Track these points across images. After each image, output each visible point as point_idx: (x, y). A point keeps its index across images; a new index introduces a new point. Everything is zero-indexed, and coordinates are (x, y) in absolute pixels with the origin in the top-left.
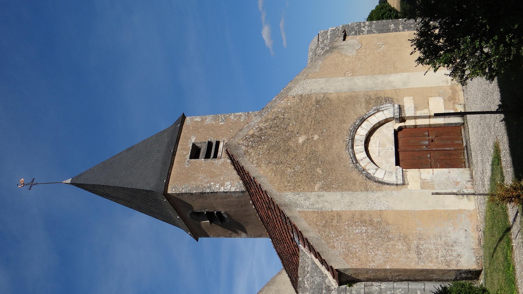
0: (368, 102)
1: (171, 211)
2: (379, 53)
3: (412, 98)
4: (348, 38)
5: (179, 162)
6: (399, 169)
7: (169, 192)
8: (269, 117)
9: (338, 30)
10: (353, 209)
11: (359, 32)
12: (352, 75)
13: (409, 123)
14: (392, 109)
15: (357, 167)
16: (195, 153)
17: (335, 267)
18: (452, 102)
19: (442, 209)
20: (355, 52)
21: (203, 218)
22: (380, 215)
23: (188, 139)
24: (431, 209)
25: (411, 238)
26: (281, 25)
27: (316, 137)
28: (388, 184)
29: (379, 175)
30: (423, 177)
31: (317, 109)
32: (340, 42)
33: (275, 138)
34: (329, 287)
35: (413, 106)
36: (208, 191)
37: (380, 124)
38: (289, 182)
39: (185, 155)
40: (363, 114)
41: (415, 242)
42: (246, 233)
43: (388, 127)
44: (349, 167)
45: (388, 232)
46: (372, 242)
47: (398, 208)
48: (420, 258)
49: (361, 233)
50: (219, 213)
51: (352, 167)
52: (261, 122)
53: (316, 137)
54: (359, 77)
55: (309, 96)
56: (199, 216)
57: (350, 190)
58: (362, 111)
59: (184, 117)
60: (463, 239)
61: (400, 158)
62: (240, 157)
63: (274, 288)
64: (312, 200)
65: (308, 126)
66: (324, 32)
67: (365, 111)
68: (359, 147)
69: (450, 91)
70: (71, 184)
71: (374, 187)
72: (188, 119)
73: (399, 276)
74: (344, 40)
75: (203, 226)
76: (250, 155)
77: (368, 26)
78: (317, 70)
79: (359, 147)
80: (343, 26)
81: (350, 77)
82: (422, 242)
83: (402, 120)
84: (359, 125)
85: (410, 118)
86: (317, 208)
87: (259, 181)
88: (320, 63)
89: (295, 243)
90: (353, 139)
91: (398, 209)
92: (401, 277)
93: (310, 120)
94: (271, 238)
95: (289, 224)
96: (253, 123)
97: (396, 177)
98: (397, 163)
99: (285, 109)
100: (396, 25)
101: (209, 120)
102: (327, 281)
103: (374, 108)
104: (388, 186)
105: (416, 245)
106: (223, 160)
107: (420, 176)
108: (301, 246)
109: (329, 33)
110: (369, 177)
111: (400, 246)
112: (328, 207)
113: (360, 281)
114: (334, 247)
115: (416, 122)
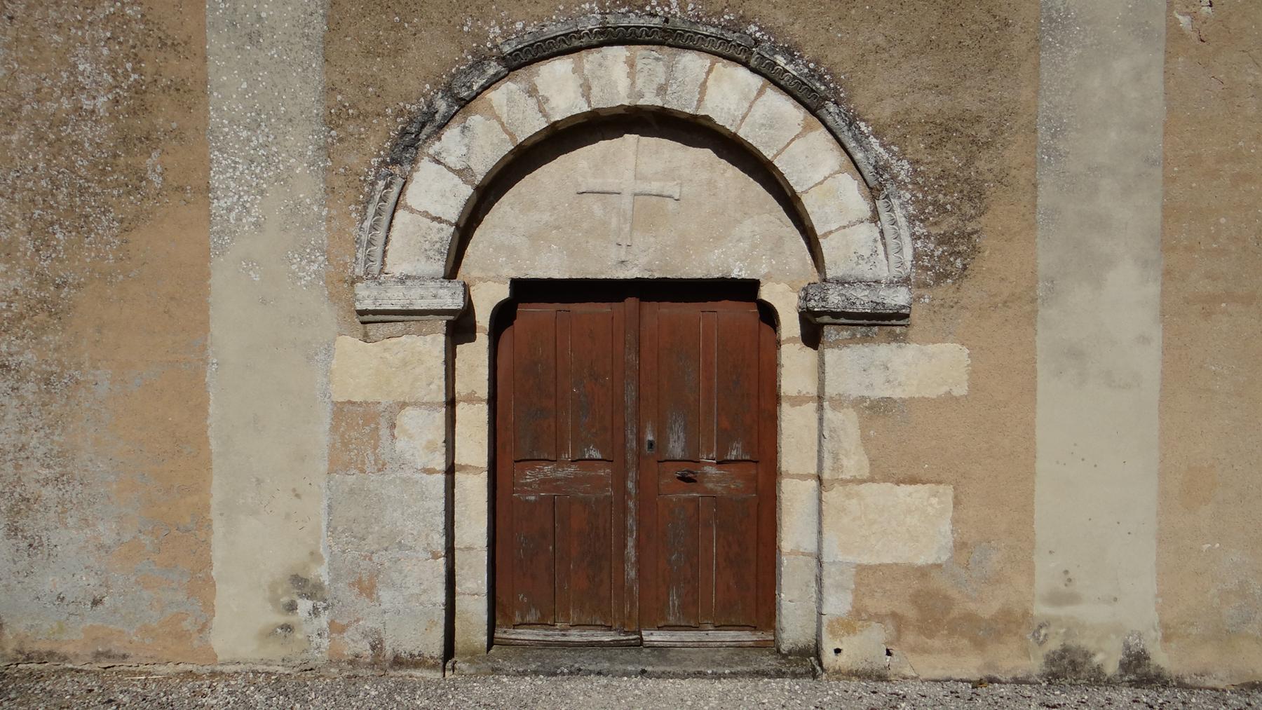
0: (943, 131)
3: (961, 390)
10: (215, 43)
12: (1175, 34)
13: (795, 365)
18: (911, 613)
19: (214, 502)
22: (181, 189)
24: (214, 445)
30: (410, 419)
35: (897, 394)
40: (862, 100)
41: (29, 355)
43: (778, 244)
44: (485, 18)
45: (82, 225)
46: (23, 143)
49: (73, 89)
51: (480, 37)
54: (1155, 79)
57: (334, 27)
58: (881, 92)
60: (50, 582)
67: (884, 112)
69: (988, 609)
71: (354, 160)
81: (1159, 22)
82: (29, 389)
84: (773, 77)
90: (670, 38)
103: (903, 169)
105: (12, 361)
107: (416, 404)
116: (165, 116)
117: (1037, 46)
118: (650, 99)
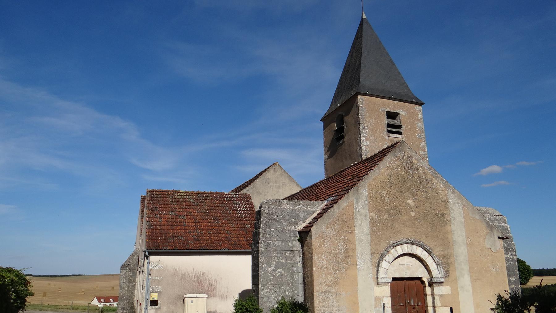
0: (444, 256)
1: (343, 99)
2: (488, 267)
4: (501, 241)
5: (383, 102)
6: (390, 281)
7: (359, 97)
8: (429, 176)
9: (507, 233)
10: (357, 243)
11: (507, 251)
12: (467, 244)
13: (428, 290)
14: (439, 276)
15: (390, 247)
16: (391, 115)
17: (313, 229)
20: (488, 246)
21: (340, 124)
23: (403, 110)
25: (337, 287)
26: (502, 182)
27: (413, 214)
28: (378, 271)
29: (384, 264)
30: (385, 299)
31: (437, 215)
32: (497, 234)
33: (410, 181)
34: (297, 224)
36: (361, 128)
37: (426, 266)
38: (376, 192)
39: (389, 107)
40: (434, 252)
41: (334, 290)
42: (328, 159)
45: (340, 270)
47: (359, 277)
48: (322, 293)
49: (339, 249)
50: (343, 137)
52: (424, 169)
53: (413, 214)
55: (447, 208)
56: (341, 121)
58: (437, 251)
59: (421, 104)
61: (398, 282)
62: (394, 153)
63: (287, 181)
64: (362, 211)
65: (422, 208)
66: (505, 220)
67: (437, 254)
68: (406, 249)
70: (362, 18)
72: (420, 108)
73: (308, 277)
74: (499, 238)
75: (332, 124)
76: (396, 161)
77: (512, 259)
78: (470, 215)
79: (406, 249)
80: (511, 237)
83: (431, 284)
84: (424, 249)
85: (433, 291)
86: (356, 215)
87: (376, 169)
88: (477, 217)
89: (327, 197)
90: (413, 244)
91: (359, 278)
92: (307, 278)
93: (427, 209)
94: (328, 179)
95: (343, 193)
96: (422, 162)
97: (384, 278)
98: (394, 279)
99: (436, 188)
100: (514, 283)
101: (420, 125)
102: (301, 222)
103: (440, 262)
104: (376, 270)
106: (387, 140)
108: (326, 202)
109: (504, 224)
110: (382, 256)
111: (330, 278)
112: (357, 223)
113: (302, 247)
114: (327, 228)
115: (429, 295)
116: (351, 253)
117: (453, 245)
118: (410, 252)
